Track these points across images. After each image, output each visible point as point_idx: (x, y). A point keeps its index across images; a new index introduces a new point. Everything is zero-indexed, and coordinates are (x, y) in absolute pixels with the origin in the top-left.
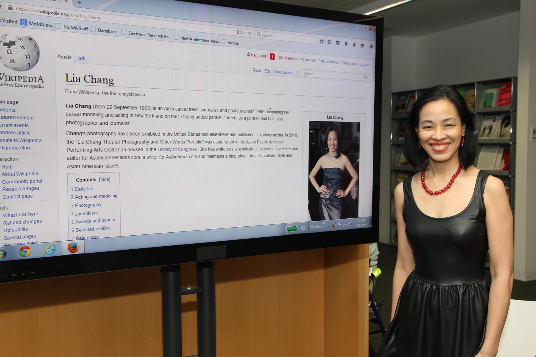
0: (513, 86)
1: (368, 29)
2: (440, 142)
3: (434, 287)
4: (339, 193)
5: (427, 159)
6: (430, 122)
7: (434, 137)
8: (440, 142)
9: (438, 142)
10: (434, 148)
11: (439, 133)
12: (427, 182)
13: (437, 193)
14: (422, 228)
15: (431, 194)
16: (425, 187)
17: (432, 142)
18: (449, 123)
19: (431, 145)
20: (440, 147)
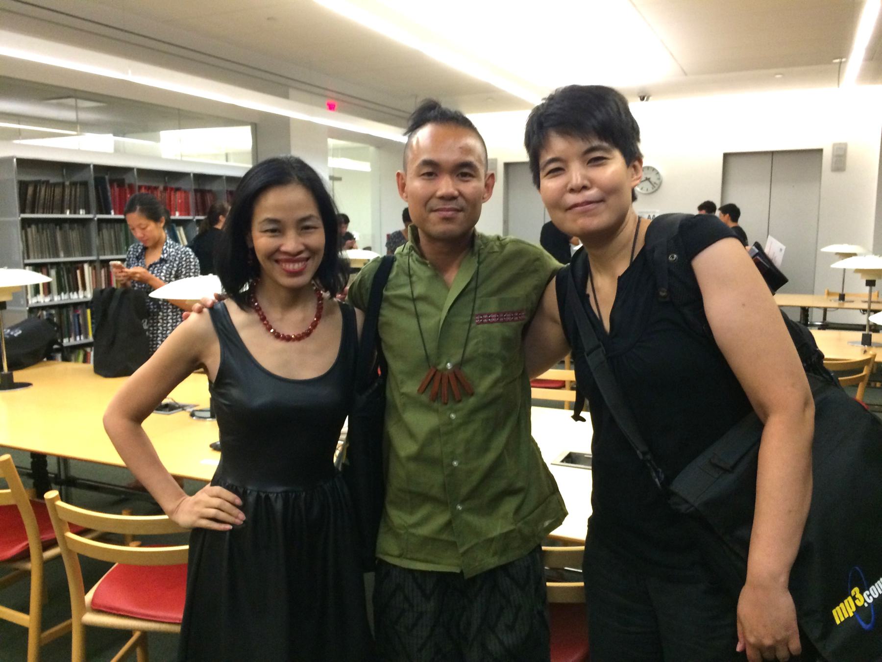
7: (283, 249)
18: (308, 223)
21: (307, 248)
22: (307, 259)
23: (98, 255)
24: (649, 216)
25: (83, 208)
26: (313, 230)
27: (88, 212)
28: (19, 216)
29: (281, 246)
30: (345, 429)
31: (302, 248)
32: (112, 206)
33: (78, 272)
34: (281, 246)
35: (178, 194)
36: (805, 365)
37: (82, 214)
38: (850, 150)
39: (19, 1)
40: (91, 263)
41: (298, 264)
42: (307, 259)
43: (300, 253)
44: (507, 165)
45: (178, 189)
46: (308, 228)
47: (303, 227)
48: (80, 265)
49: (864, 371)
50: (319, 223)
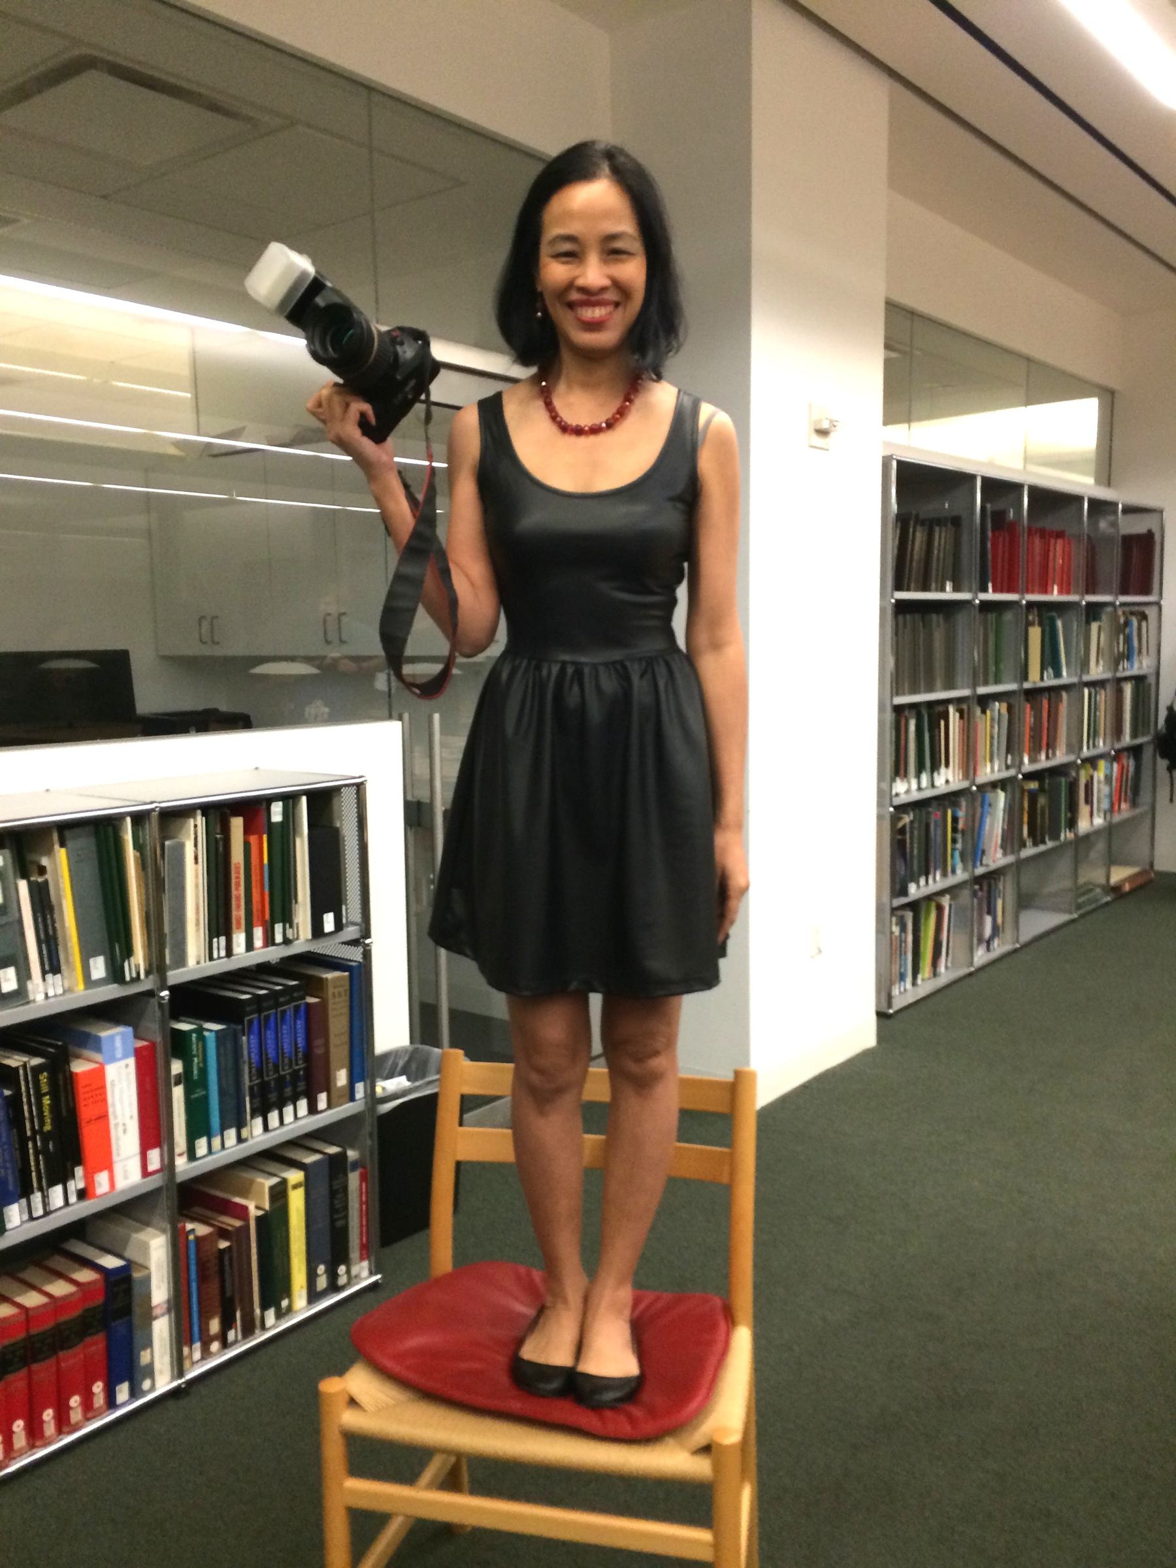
0: (1023, 505)
1: (990, 809)
2: (593, 299)
3: (570, 670)
4: (356, 905)
5: (539, 305)
6: (570, 238)
7: (580, 282)
8: (593, 299)
9: (591, 296)
10: (579, 316)
11: (594, 274)
12: (557, 403)
13: (578, 431)
14: (534, 519)
15: (565, 429)
16: (554, 417)
17: (575, 296)
18: (618, 245)
19: (571, 306)
20: (593, 312)
21: (617, 285)
22: (617, 305)
23: (974, 686)
25: (950, 581)
26: (624, 257)
27: (956, 589)
28: (892, 597)
29: (576, 277)
30: (238, 1315)
31: (606, 282)
32: (990, 577)
33: (942, 723)
34: (576, 277)
35: (1060, 542)
36: (183, 1386)
37: (949, 594)
39: (164, 3)
40: (959, 701)
41: (600, 310)
42: (617, 305)
43: (603, 289)
45: (1060, 535)
46: (617, 252)
47: (612, 251)
48: (941, 708)
49: (156, 818)
50: (636, 246)
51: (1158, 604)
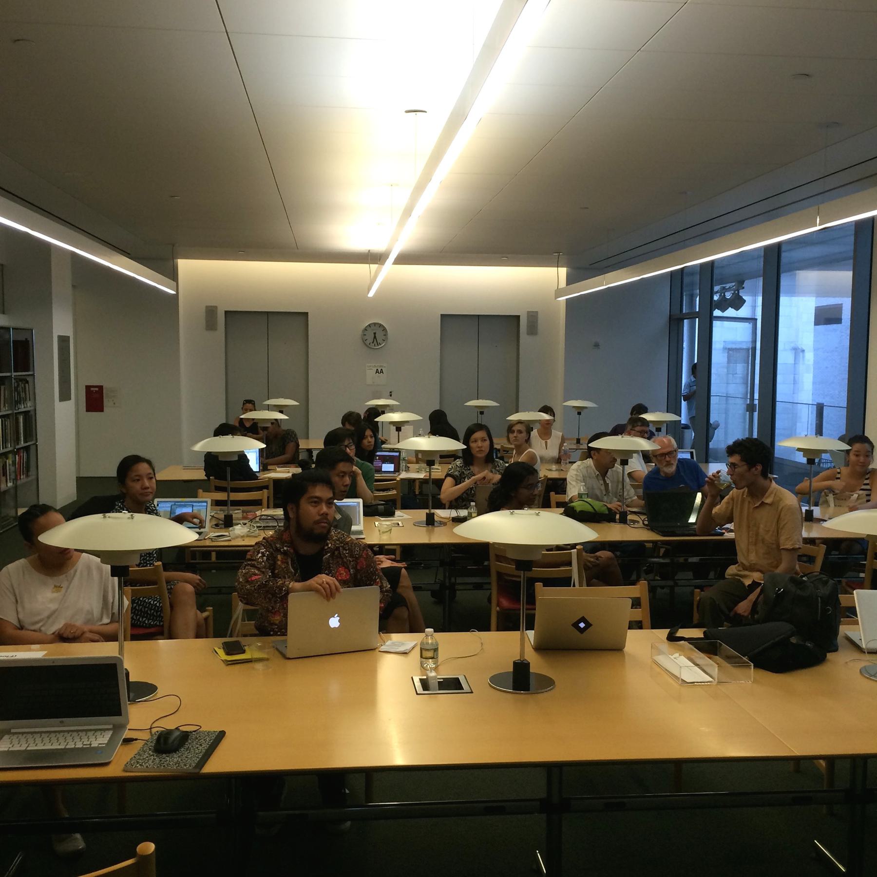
24: (377, 370)
38: (539, 316)
44: (226, 312)
51: (33, 375)
